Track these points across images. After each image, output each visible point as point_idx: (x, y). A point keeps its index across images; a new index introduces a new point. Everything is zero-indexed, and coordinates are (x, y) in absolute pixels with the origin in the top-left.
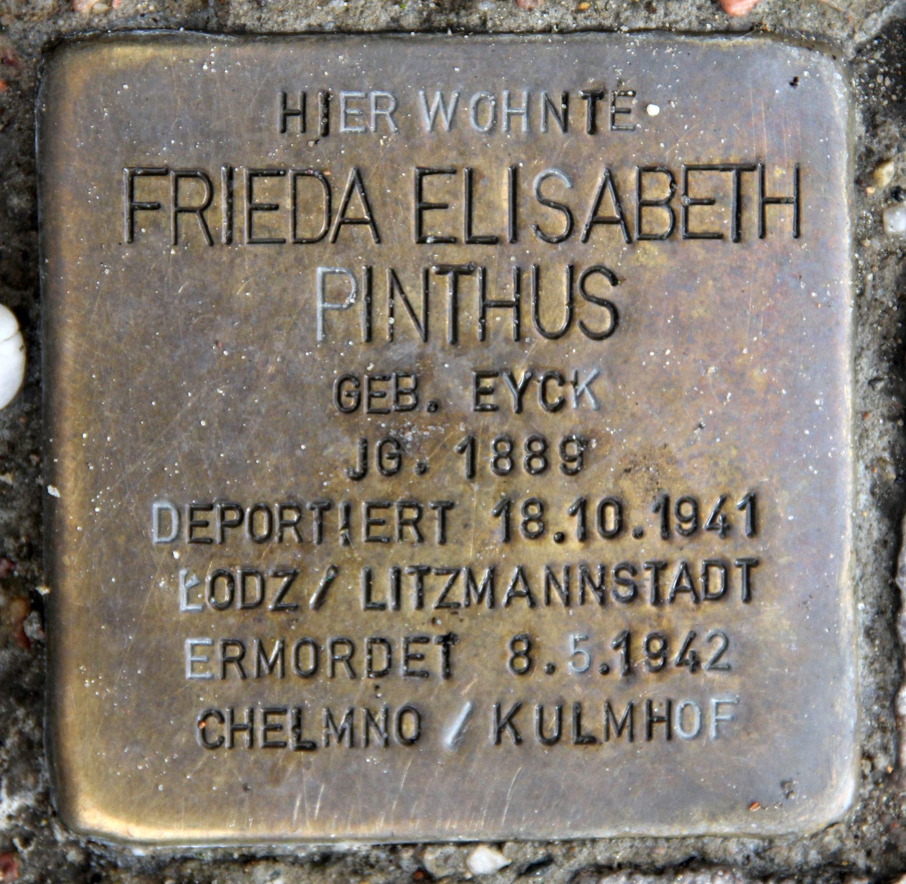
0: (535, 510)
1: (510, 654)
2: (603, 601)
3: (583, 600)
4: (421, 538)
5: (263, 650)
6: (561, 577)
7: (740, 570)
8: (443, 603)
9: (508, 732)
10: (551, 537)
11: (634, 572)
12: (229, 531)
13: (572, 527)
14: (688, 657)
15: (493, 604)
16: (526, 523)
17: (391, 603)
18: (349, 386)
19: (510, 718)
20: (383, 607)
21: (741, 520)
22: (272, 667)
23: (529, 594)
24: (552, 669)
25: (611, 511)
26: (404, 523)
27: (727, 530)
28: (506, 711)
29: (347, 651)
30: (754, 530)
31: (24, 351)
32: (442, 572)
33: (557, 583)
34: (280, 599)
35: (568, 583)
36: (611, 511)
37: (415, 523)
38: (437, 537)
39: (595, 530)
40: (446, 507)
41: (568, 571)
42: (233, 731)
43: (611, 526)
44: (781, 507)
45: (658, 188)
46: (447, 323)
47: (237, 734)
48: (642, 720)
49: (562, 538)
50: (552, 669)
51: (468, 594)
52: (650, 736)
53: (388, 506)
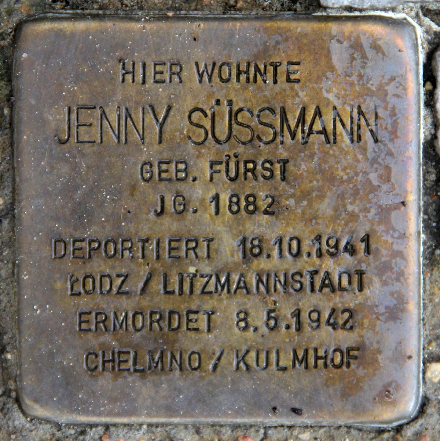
1: (237, 319)
3: (275, 290)
7: (357, 276)
9: (242, 364)
10: (305, 257)
11: (302, 276)
14: (242, 284)
15: (229, 291)
16: (251, 249)
18: (147, 167)
19: (243, 358)
20: (173, 292)
22: (121, 326)
23: (246, 287)
24: (256, 329)
25: (294, 244)
26: (188, 249)
28: (241, 355)
31: (436, 99)
33: (262, 283)
34: (120, 287)
37: (194, 249)
39: (287, 253)
41: (268, 276)
42: (104, 362)
46: (124, 137)
47: (106, 365)
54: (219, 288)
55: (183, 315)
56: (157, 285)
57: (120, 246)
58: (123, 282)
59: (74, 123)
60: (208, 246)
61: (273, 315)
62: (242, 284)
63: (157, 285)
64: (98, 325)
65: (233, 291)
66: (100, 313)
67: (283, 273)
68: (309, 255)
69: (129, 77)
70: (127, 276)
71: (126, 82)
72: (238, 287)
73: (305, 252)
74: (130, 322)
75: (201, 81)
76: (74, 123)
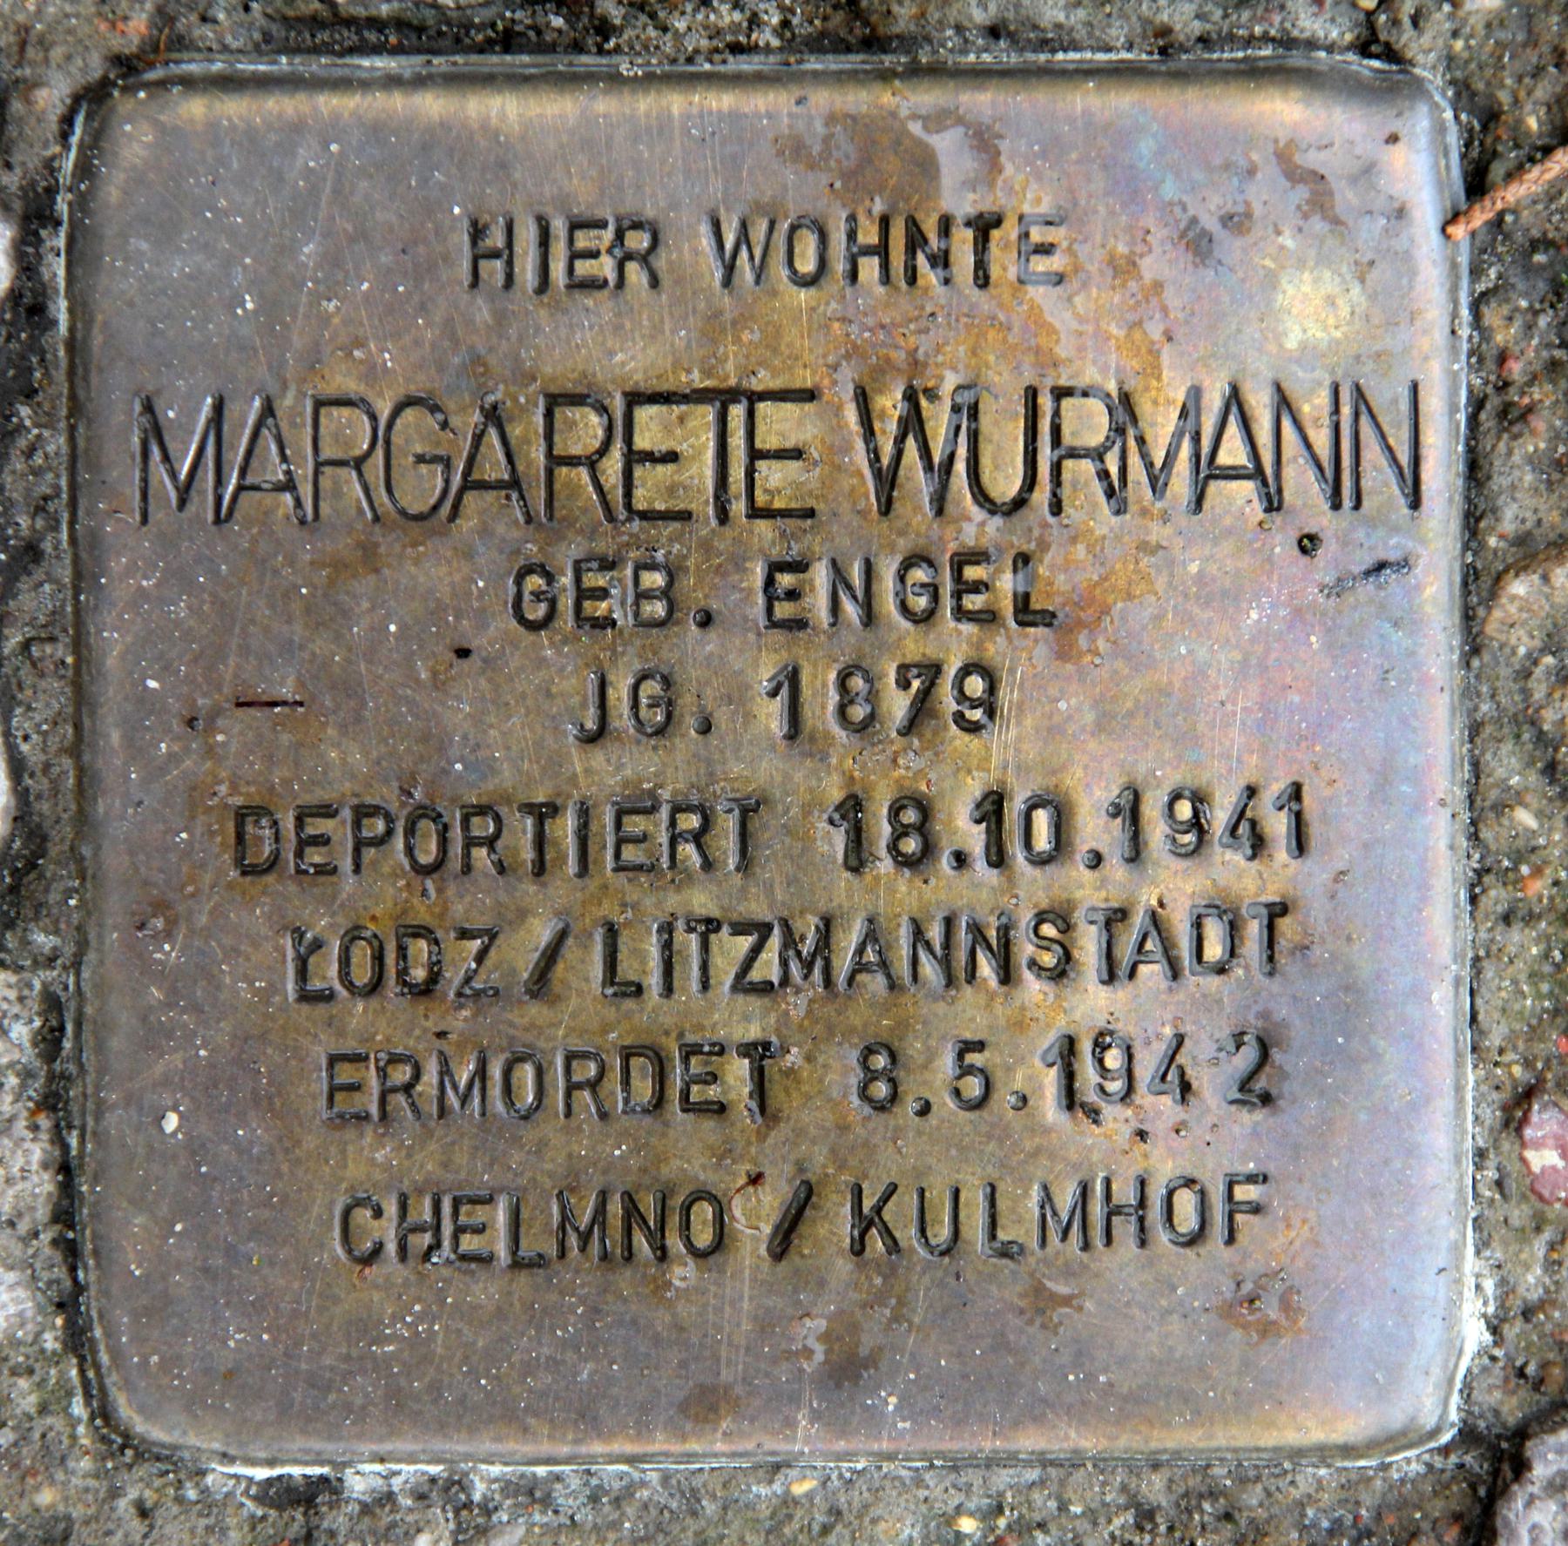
0: (910, 816)
2: (1007, 975)
4: (708, 865)
5: (445, 1071)
6: (935, 933)
8: (742, 985)
10: (945, 862)
12: (369, 854)
13: (975, 839)
14: (870, 956)
15: (828, 981)
17: (654, 981)
19: (878, 1210)
20: (639, 990)
21: (1278, 825)
24: (925, 1110)
25: (1042, 819)
27: (1259, 844)
29: (592, 1069)
30: (1300, 844)
32: (740, 929)
35: (947, 945)
36: (1042, 819)
38: (732, 862)
40: (748, 810)
43: (1042, 842)
44: (1338, 807)
45: (585, 429)
48: (1097, 1209)
49: (961, 860)
50: (925, 1110)
51: (784, 963)
52: (1109, 1239)
53: (652, 810)
54: (795, 969)
55: (613, 1068)
56: (585, 967)
57: (456, 833)
58: (481, 957)
59: (737, 441)
60: (743, 825)
61: (973, 1058)
62: (870, 956)
63: (585, 967)
64: (576, 1094)
65: (841, 977)
66: (585, 1056)
67: (940, 916)
68: (961, 859)
69: (494, 269)
70: (493, 936)
71: (517, 287)
72: (860, 967)
73: (1086, 848)
74: (496, 1091)
75: (727, 282)
76: (737, 441)
